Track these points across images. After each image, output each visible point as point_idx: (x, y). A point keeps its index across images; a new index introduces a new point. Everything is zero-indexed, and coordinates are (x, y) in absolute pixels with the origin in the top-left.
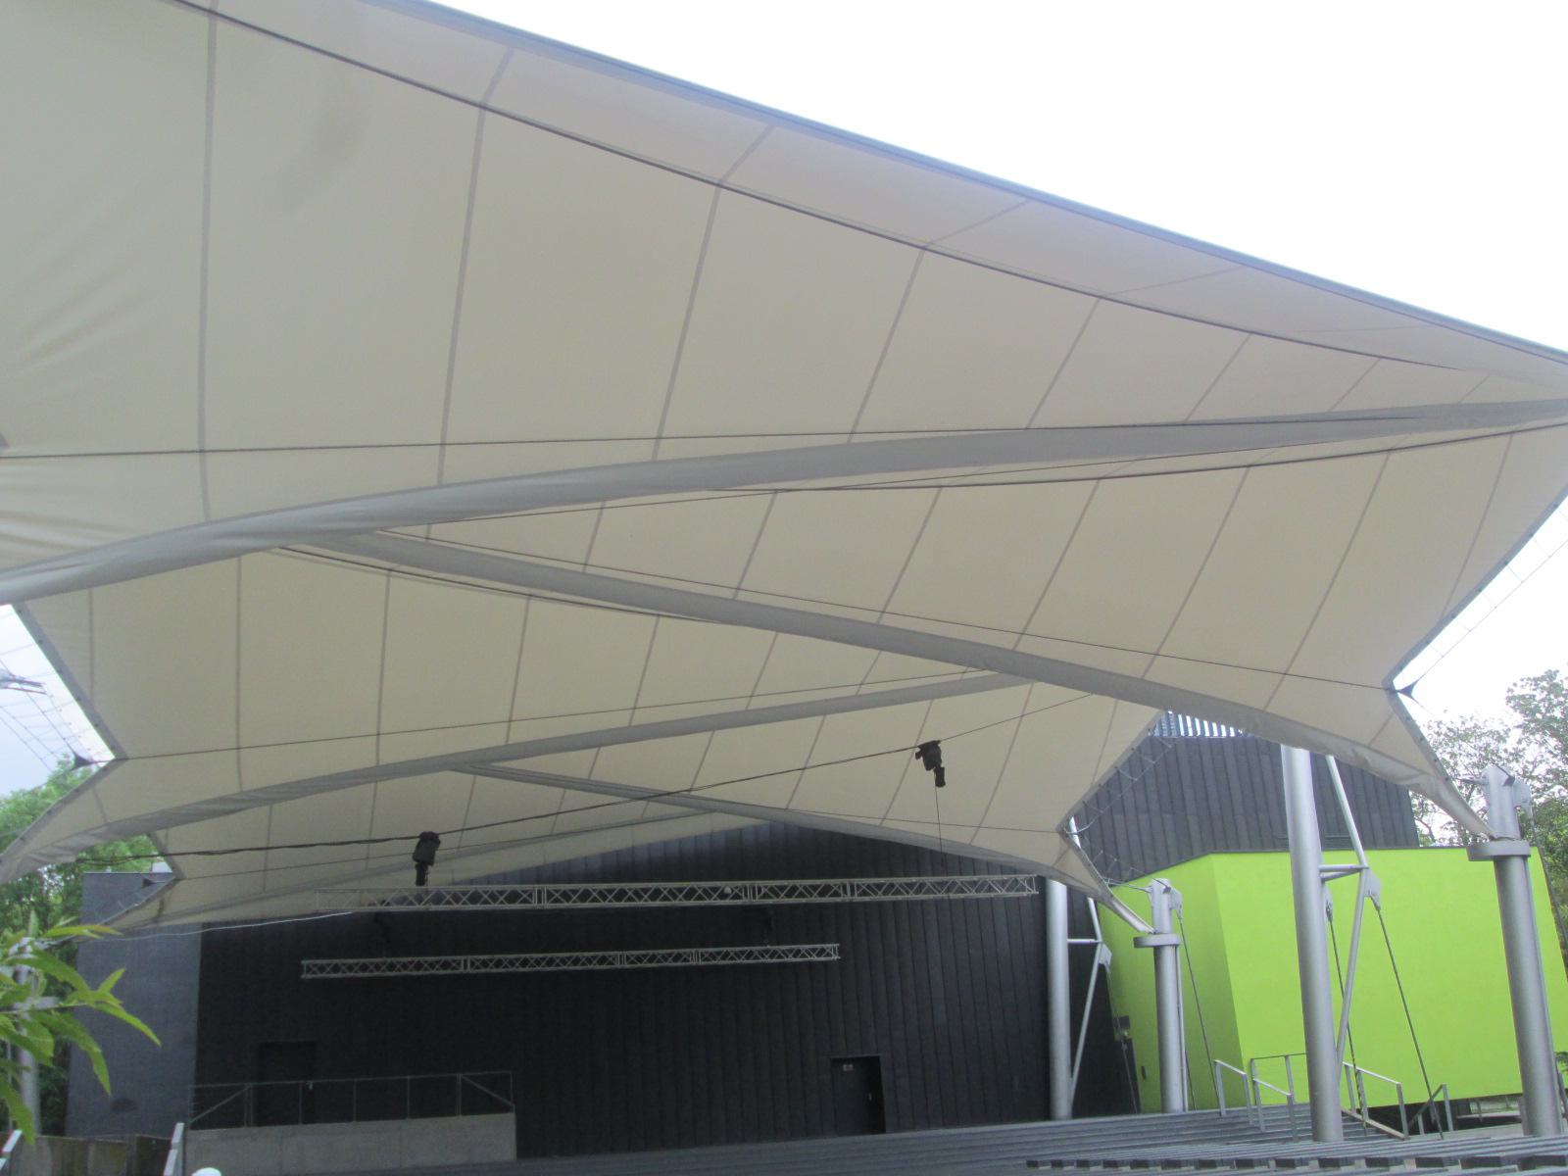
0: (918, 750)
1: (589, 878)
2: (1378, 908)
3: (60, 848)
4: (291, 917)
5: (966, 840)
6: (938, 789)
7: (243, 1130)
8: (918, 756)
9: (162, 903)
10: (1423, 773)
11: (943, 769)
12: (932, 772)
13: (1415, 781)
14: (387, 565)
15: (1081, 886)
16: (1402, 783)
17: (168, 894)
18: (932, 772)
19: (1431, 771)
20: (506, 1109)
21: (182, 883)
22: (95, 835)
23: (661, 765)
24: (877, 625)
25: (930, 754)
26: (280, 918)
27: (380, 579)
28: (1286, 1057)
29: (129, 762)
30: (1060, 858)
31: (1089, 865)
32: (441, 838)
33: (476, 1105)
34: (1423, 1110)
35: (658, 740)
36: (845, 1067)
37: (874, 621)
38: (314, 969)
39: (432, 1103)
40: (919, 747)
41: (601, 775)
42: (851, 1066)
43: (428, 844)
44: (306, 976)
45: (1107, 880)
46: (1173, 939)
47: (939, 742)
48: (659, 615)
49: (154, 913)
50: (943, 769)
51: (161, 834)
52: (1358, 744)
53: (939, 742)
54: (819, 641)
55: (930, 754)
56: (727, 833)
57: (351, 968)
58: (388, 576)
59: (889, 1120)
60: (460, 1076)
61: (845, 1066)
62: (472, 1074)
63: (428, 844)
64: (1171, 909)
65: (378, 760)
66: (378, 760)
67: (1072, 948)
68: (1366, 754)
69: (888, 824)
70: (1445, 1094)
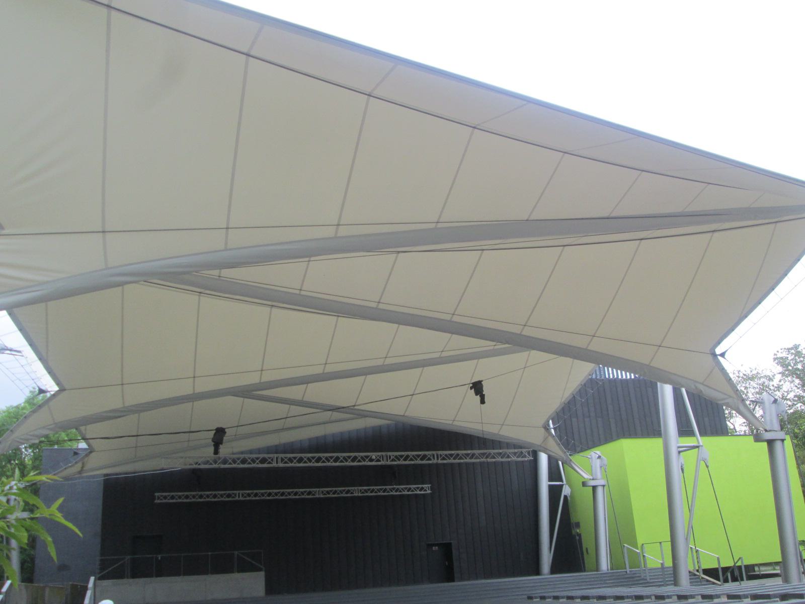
0: (471, 385)
1: (302, 451)
2: (707, 467)
3: (31, 435)
4: (149, 471)
5: (496, 432)
6: (482, 405)
7: (125, 581)
8: (471, 388)
9: (83, 464)
10: (731, 397)
11: (484, 395)
12: (478, 396)
13: (726, 401)
14: (199, 290)
15: (555, 455)
16: (720, 402)
17: (86, 459)
18: (478, 396)
19: (735, 396)
20: (260, 570)
21: (93, 454)
22: (49, 429)
23: (339, 393)
24: (450, 321)
25: (477, 387)
26: (144, 472)
27: (195, 297)
28: (660, 543)
29: (66, 392)
30: (544, 441)
31: (559, 444)
32: (226, 430)
33: (245, 567)
34: (730, 570)
35: (338, 380)
36: (434, 548)
37: (449, 319)
38: (161, 498)
39: (222, 567)
40: (472, 383)
41: (308, 398)
42: (437, 547)
43: (220, 434)
44: (157, 501)
45: (568, 452)
46: (602, 482)
47: (482, 381)
48: (338, 316)
49: (79, 469)
50: (484, 395)
51: (82, 428)
52: (697, 382)
53: (482, 381)
54: (421, 329)
55: (477, 387)
56: (373, 428)
57: (180, 497)
58: (199, 296)
59: (456, 575)
60: (236, 553)
61: (434, 548)
62: (242, 552)
63: (220, 434)
64: (601, 467)
65: (194, 391)
66: (194, 391)
67: (550, 487)
68: (701, 387)
69: (456, 423)
70: (742, 562)
